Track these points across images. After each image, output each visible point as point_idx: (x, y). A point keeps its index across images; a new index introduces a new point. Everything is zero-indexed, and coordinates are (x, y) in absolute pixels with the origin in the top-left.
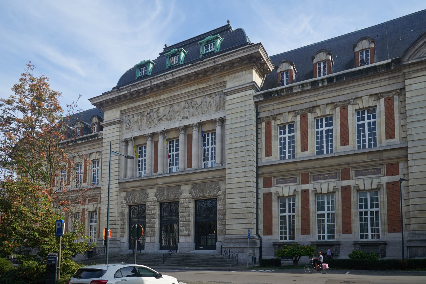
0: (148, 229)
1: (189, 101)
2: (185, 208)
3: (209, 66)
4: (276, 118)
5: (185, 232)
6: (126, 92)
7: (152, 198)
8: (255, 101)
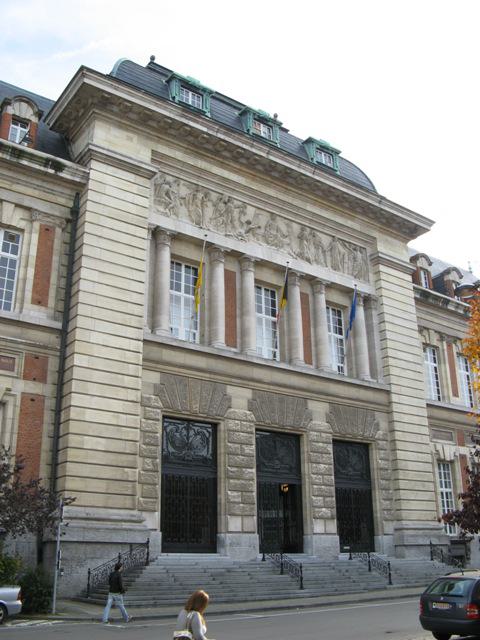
0: (235, 494)
2: (322, 453)
5: (324, 509)
7: (239, 413)
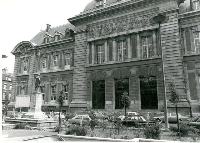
1: (149, 16)
3: (83, 17)
4: (192, 28)
6: (84, 17)
8: (179, 18)
